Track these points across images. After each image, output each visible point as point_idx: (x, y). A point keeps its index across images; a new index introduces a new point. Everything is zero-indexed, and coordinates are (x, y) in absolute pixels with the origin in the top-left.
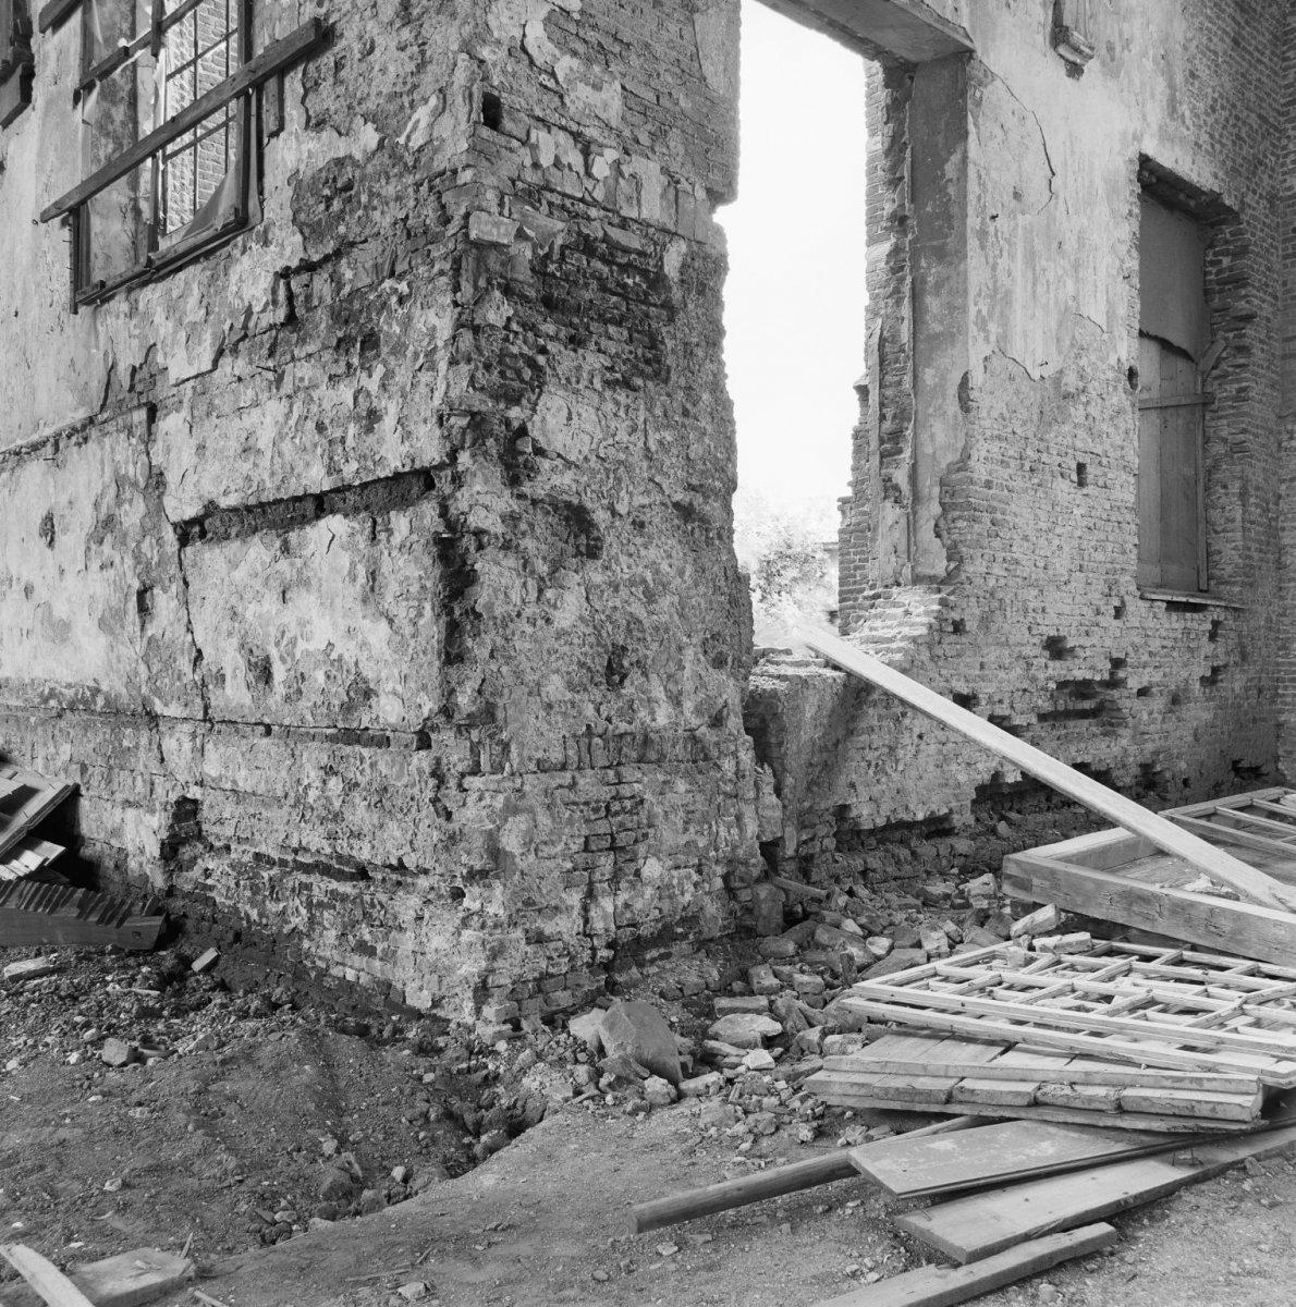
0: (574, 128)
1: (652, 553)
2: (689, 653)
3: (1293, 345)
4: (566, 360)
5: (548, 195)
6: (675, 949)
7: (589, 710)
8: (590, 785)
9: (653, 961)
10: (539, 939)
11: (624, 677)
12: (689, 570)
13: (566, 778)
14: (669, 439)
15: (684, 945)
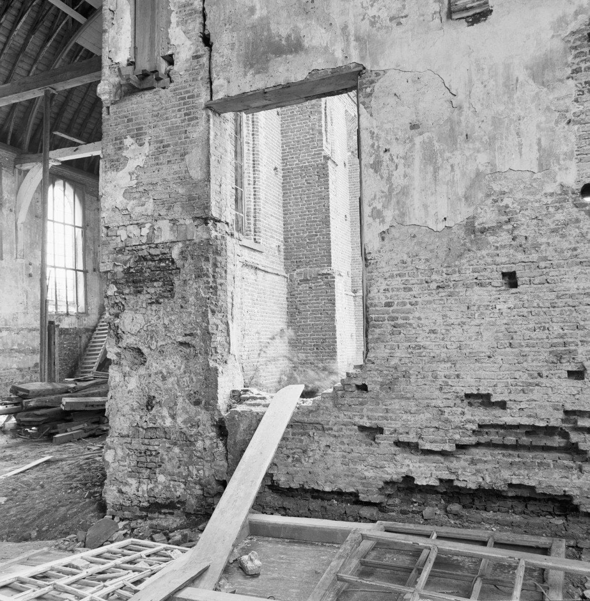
0: (135, 222)
1: (168, 362)
2: (180, 400)
3: (588, 64)
4: (132, 299)
5: (127, 248)
6: (175, 512)
7: (138, 418)
8: (136, 444)
9: (165, 514)
10: (120, 491)
11: (152, 407)
12: (183, 367)
13: (129, 440)
14: (173, 318)
15: (179, 512)
